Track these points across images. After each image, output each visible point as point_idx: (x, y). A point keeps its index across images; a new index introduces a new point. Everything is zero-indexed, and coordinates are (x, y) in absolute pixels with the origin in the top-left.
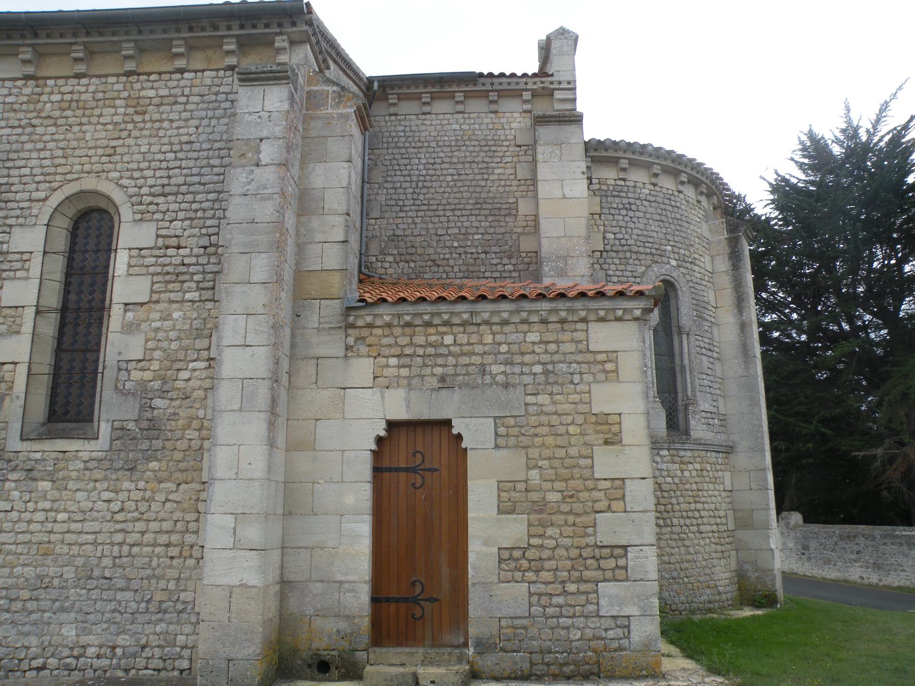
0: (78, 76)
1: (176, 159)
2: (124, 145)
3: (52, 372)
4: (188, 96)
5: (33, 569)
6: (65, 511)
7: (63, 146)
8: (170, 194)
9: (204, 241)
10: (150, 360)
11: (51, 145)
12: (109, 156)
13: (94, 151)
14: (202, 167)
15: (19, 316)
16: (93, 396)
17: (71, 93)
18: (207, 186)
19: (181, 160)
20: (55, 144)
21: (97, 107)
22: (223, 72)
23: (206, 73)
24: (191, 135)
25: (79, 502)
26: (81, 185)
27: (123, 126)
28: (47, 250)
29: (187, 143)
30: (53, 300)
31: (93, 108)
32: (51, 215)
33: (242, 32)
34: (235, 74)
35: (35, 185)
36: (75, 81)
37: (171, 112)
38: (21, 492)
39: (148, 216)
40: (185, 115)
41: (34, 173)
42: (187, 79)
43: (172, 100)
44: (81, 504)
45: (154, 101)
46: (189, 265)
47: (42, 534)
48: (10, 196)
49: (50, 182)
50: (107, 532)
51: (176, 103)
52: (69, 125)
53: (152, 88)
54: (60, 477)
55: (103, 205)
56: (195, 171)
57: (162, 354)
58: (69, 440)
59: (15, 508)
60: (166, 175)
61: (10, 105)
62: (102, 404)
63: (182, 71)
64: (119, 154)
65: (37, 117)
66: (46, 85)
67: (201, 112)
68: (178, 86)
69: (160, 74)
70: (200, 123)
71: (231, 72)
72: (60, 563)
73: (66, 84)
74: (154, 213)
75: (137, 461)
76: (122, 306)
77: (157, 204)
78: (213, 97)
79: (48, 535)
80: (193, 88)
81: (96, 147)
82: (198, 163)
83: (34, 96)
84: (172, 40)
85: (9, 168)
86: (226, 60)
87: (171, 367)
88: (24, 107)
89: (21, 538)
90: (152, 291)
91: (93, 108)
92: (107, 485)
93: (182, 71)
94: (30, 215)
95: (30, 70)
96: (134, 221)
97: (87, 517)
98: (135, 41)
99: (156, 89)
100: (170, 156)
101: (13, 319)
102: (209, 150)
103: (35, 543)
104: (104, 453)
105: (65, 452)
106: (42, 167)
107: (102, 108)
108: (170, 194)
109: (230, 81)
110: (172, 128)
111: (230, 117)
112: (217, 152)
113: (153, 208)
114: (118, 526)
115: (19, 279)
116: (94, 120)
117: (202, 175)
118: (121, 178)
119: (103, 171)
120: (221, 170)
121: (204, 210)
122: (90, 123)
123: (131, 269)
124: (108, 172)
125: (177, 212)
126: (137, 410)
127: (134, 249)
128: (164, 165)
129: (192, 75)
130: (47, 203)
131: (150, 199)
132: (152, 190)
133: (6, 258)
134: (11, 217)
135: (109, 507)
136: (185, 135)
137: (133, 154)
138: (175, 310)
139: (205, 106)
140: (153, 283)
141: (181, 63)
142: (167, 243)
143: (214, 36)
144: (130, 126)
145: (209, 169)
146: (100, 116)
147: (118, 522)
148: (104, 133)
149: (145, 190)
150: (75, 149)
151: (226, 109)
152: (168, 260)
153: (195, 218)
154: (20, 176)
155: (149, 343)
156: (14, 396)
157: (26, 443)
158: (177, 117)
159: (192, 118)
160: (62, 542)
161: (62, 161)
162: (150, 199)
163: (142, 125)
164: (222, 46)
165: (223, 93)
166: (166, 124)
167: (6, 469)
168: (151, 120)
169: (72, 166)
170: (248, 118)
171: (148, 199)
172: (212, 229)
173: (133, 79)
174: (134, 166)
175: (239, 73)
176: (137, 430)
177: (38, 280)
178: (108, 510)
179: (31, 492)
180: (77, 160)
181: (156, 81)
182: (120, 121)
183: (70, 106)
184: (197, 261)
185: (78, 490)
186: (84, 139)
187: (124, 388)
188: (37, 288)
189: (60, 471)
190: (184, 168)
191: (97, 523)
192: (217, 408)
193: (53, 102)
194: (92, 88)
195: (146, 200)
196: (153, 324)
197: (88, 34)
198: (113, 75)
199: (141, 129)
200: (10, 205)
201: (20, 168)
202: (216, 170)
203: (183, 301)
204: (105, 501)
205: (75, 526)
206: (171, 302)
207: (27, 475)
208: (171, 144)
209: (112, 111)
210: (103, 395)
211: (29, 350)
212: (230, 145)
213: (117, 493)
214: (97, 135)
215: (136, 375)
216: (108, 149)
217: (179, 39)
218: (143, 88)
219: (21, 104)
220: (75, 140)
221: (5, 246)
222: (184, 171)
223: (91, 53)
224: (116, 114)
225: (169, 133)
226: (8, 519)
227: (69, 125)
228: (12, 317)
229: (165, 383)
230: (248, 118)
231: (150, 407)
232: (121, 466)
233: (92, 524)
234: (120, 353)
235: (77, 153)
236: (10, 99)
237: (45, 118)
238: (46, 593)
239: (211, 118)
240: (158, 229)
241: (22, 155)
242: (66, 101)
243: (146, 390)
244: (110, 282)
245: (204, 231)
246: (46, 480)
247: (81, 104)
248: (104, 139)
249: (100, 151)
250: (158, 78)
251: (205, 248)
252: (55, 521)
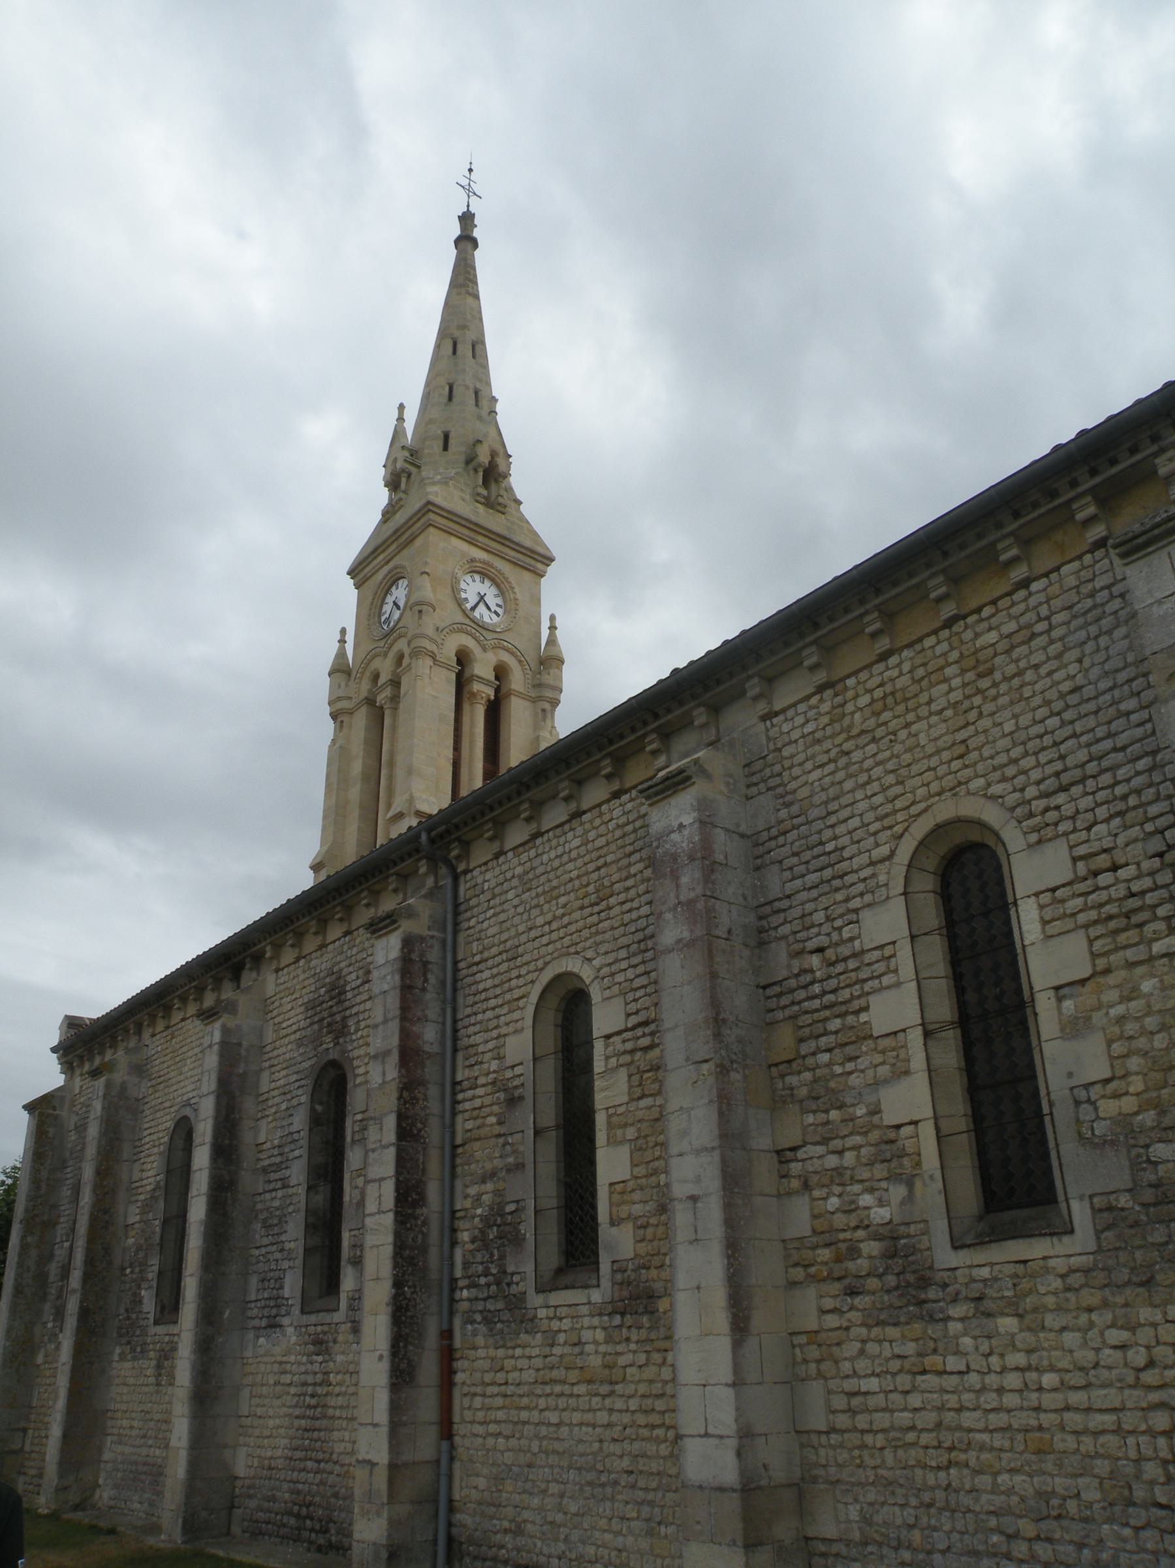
0: (883, 657)
1: (1063, 723)
2: (977, 733)
3: (972, 1127)
4: (1048, 618)
5: (1028, 1479)
6: (1052, 1369)
7: (892, 768)
8: (1072, 784)
9: (1156, 845)
10: (1124, 1077)
11: (877, 772)
12: (961, 756)
13: (937, 758)
14: (1109, 722)
15: (902, 1047)
16: (1046, 1156)
17: (881, 685)
18: (1129, 750)
19: (1072, 722)
20: (881, 768)
21: (922, 691)
22: (1088, 556)
23: (1065, 570)
24: (1075, 676)
25: (1071, 1351)
26: (934, 817)
27: (967, 704)
28: (915, 932)
29: (1072, 692)
30: (944, 1009)
31: (916, 695)
32: (906, 877)
33: (1098, 480)
34: (1111, 550)
35: (872, 839)
36: (880, 667)
37: (1031, 653)
38: (975, 1338)
39: (1049, 832)
40: (1053, 650)
41: (866, 821)
42: (1037, 592)
43: (1025, 633)
44: (1075, 1354)
45: (1000, 647)
46: (1143, 893)
47: (1025, 1413)
48: (845, 865)
49: (890, 827)
50: (1136, 1408)
51: (1033, 636)
52: (891, 733)
53: (990, 629)
54: (1028, 1307)
55: (975, 836)
56: (1100, 732)
57: (1141, 1061)
58: (1029, 1240)
59: (973, 1367)
60: (1057, 756)
61: (811, 737)
62: (1064, 1168)
63: (1025, 584)
64: (974, 749)
65: (847, 740)
66: (846, 689)
67: (1077, 635)
68: (1027, 610)
69: (994, 602)
70: (1082, 651)
71: (1103, 550)
72: (1070, 1469)
73: (872, 676)
74: (1056, 824)
75: (1153, 1265)
76: (1052, 993)
77: (1057, 808)
78: (1089, 603)
79: (1034, 1414)
80: (1052, 602)
81: (938, 752)
82: (1103, 717)
83: (836, 711)
84: (993, 544)
85: (832, 826)
86: (1088, 535)
87: (1166, 1082)
88: (829, 731)
89: (996, 1420)
90: (1094, 956)
91: (916, 695)
92: (1110, 1316)
93: (1025, 584)
94: (878, 886)
95: (821, 677)
96: (1030, 846)
97: (1093, 1380)
98: (943, 571)
99: (997, 628)
100: (1053, 722)
101: (895, 1053)
102: (1111, 689)
103: (1019, 1430)
104: (1091, 1257)
105: (1025, 1262)
106: (874, 808)
107: (929, 689)
108: (1072, 784)
109: (1108, 563)
110: (1040, 678)
111: (1127, 622)
112: (1126, 687)
113: (1052, 816)
114: (1155, 1397)
115: (888, 988)
116: (923, 711)
117: (1115, 734)
118: (989, 785)
119: (960, 784)
120: (1145, 714)
121: (1138, 792)
122: (919, 719)
123: (1047, 927)
124: (967, 783)
125: (1093, 810)
126: (1127, 1172)
127: (1043, 892)
128: (1048, 740)
129: (1043, 582)
130: (896, 859)
131: (1042, 803)
132: (1042, 787)
133: (862, 962)
134: (854, 897)
135: (1125, 1358)
136: (1064, 680)
137: (994, 742)
138: (1141, 977)
139: (1081, 621)
140: (1091, 942)
141: (1019, 572)
142: (1093, 867)
143: (1055, 508)
144: (977, 700)
145: (1122, 721)
146: (930, 702)
147: (1149, 1388)
148: (944, 725)
149: (1031, 791)
150: (909, 765)
151: (1116, 612)
152: (1103, 896)
153: (1127, 811)
154: (850, 832)
155: (1114, 1046)
156: (926, 1177)
157: (963, 1253)
158: (1043, 658)
159: (1067, 649)
160: (1062, 1427)
161: (898, 790)
162: (1042, 803)
163: (993, 692)
164: (1073, 517)
165: (1103, 588)
166: (1029, 676)
167: (944, 1299)
168: (1006, 679)
169: (913, 792)
170: (1157, 611)
171: (1041, 804)
172: (1163, 818)
173: (959, 627)
174: (1002, 759)
175: (1115, 547)
176: (1137, 1208)
177: (914, 984)
178: (1126, 1365)
179: (989, 1337)
180: (917, 781)
181: (993, 615)
182: (960, 697)
183: (885, 705)
184: (1155, 882)
185: (1064, 1329)
186: (918, 745)
187: (1093, 1134)
188: (916, 995)
189: (1026, 1296)
190: (1082, 734)
191: (1113, 1391)
192: (1086, 1405)
193: (861, 709)
194: (906, 667)
195: (1037, 806)
196: (1113, 1012)
197: (878, 592)
198: (928, 635)
199: (995, 699)
200: (848, 879)
201: (846, 820)
202: (1134, 718)
203: (1151, 959)
204: (1115, 1347)
205: (1076, 1398)
206: (1131, 965)
207: (976, 1308)
208: (1048, 703)
209: (944, 687)
210: (1062, 1153)
211: (929, 1097)
212: (1143, 668)
213: (1133, 1330)
214: (934, 733)
215: (1108, 1107)
216: (955, 748)
217: (1005, 537)
218: (977, 635)
219: (824, 729)
220: (905, 751)
221: (857, 943)
222: (1083, 739)
223: (889, 617)
224: (951, 690)
225: (1038, 687)
226: (967, 1385)
227: (891, 733)
228: (893, 1049)
229: (1163, 1113)
230: (1157, 611)
231: (1149, 1161)
232: (1126, 1278)
233: (1104, 1392)
234: (1070, 1075)
235: (915, 769)
236: (809, 728)
237: (859, 735)
238: (1062, 1528)
239: (1096, 638)
240: (1071, 847)
241: (844, 801)
242: (877, 700)
243: (1133, 1131)
244: (1020, 958)
245: (1149, 827)
246: (1008, 1315)
247: (899, 696)
248: (945, 734)
249: (946, 755)
250: (993, 611)
251: (1161, 855)
252: (1040, 1389)
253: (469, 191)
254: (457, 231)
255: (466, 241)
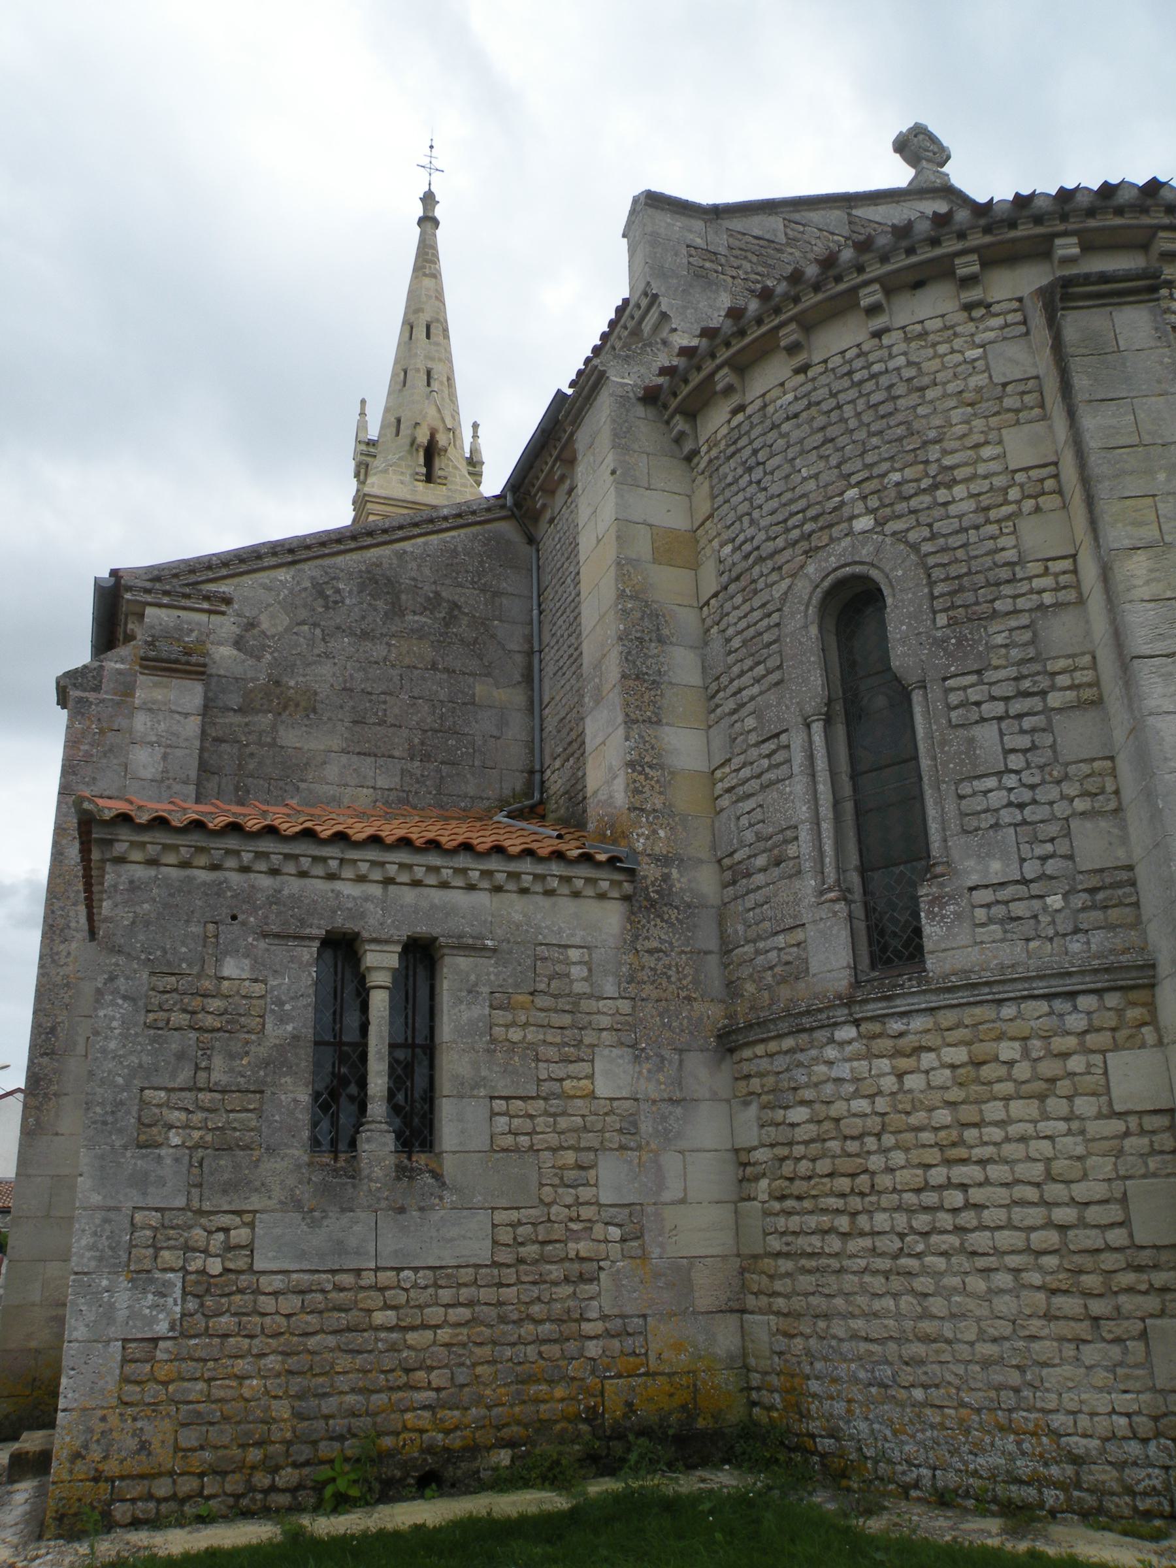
253: (430, 168)
254: (420, 212)
255: (428, 221)
